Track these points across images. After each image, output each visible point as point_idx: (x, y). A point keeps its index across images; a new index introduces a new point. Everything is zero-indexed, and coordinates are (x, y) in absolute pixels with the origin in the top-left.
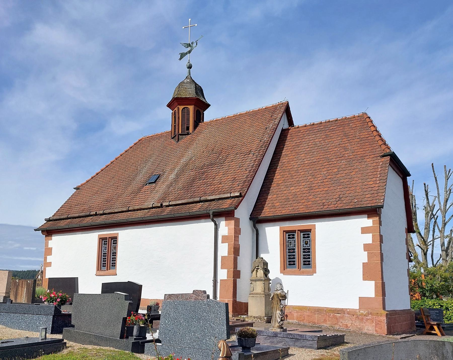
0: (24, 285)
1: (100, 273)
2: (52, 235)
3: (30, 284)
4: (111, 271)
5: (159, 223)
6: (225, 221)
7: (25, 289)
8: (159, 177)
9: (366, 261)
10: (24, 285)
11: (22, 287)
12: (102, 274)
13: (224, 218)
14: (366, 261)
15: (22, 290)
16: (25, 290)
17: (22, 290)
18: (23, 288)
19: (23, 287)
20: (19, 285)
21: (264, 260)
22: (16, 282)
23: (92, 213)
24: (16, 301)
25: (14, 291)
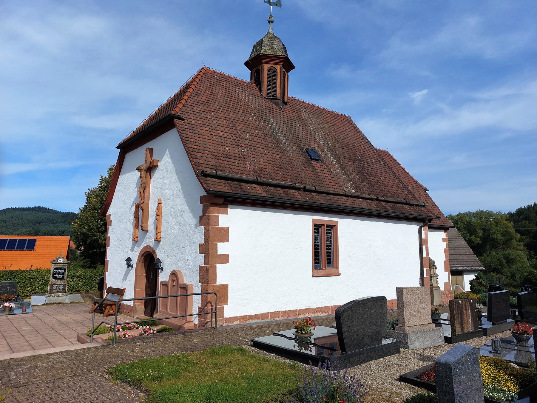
0: (467, 306)
1: (319, 274)
2: (228, 205)
3: (473, 304)
4: (329, 269)
5: (269, 209)
6: (229, 209)
7: (470, 312)
8: (318, 160)
9: (445, 260)
10: (467, 306)
11: (466, 310)
12: (321, 274)
13: (443, 231)
14: (445, 260)
15: (466, 314)
16: (470, 313)
17: (466, 314)
18: (467, 311)
19: (467, 309)
20: (462, 307)
21: (431, 259)
22: (459, 303)
23: (299, 185)
24: (463, 331)
25: (458, 318)
